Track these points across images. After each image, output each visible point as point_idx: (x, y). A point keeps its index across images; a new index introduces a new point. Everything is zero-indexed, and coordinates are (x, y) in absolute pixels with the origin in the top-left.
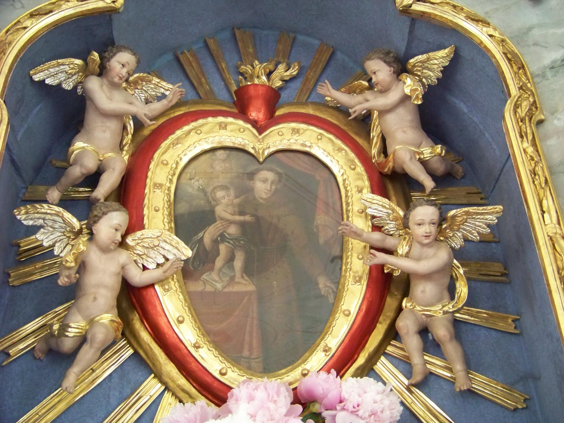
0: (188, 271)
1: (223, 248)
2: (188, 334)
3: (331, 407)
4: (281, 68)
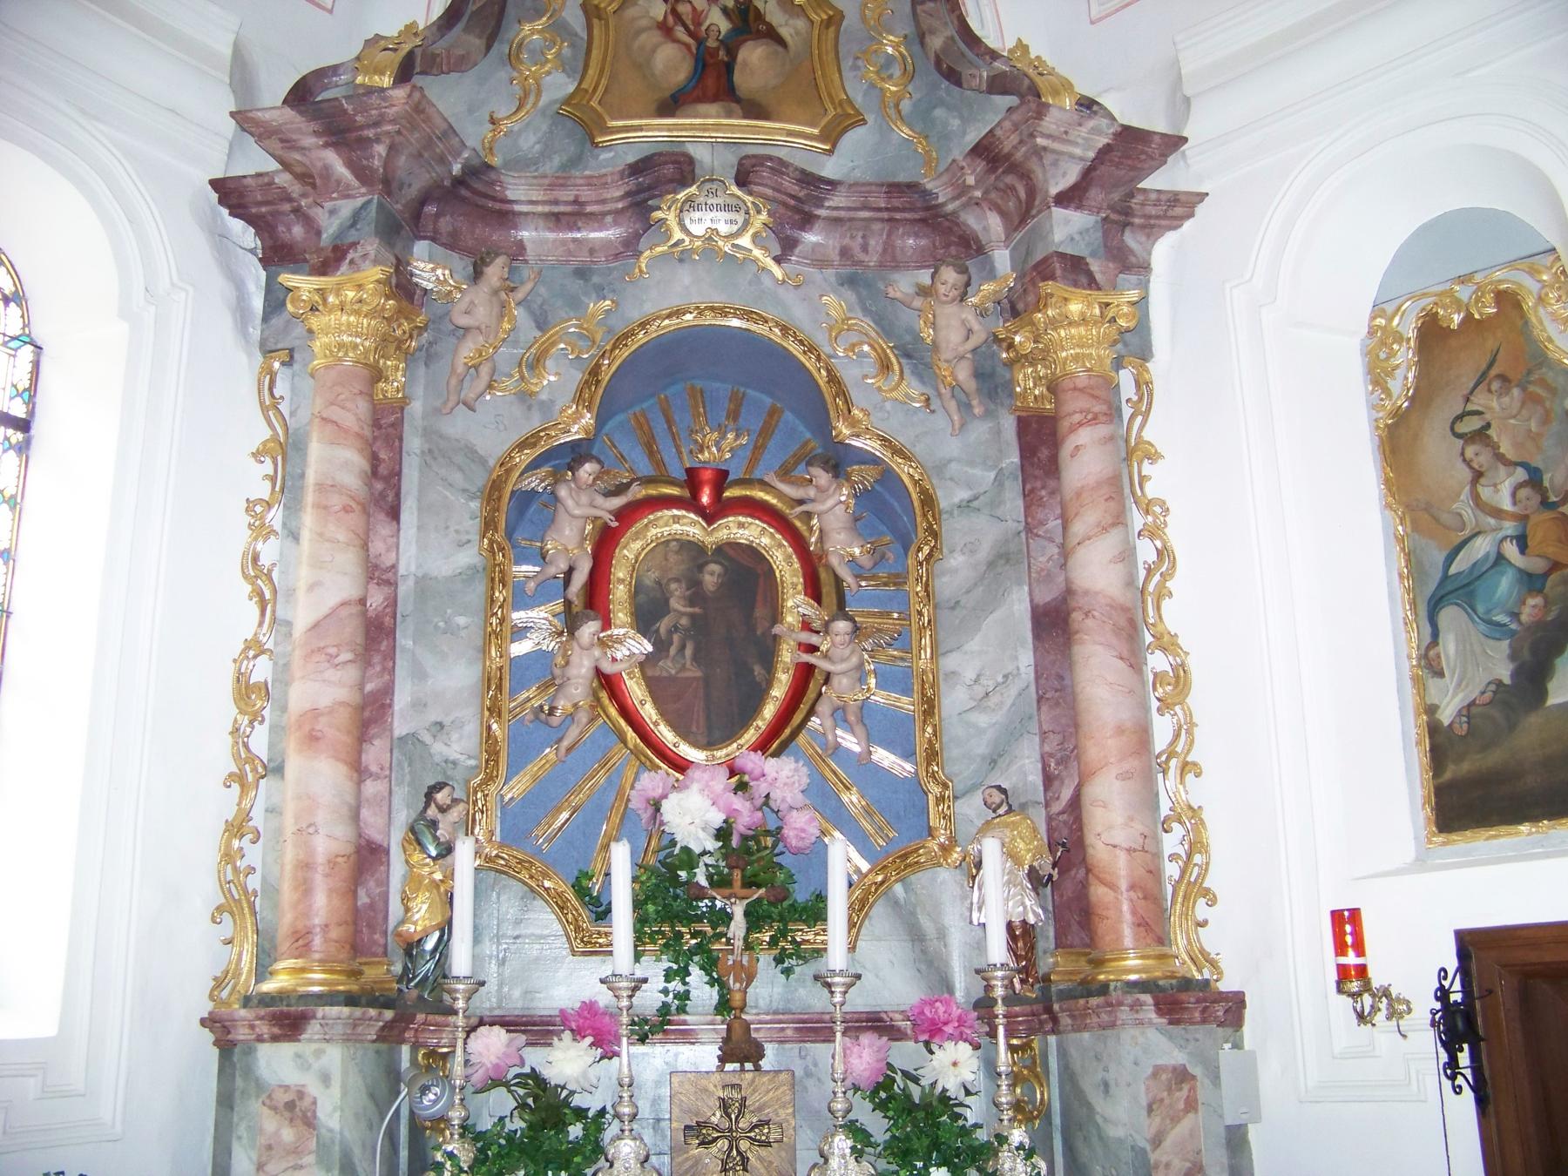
0: (646, 664)
1: (676, 637)
2: (649, 712)
3: (757, 779)
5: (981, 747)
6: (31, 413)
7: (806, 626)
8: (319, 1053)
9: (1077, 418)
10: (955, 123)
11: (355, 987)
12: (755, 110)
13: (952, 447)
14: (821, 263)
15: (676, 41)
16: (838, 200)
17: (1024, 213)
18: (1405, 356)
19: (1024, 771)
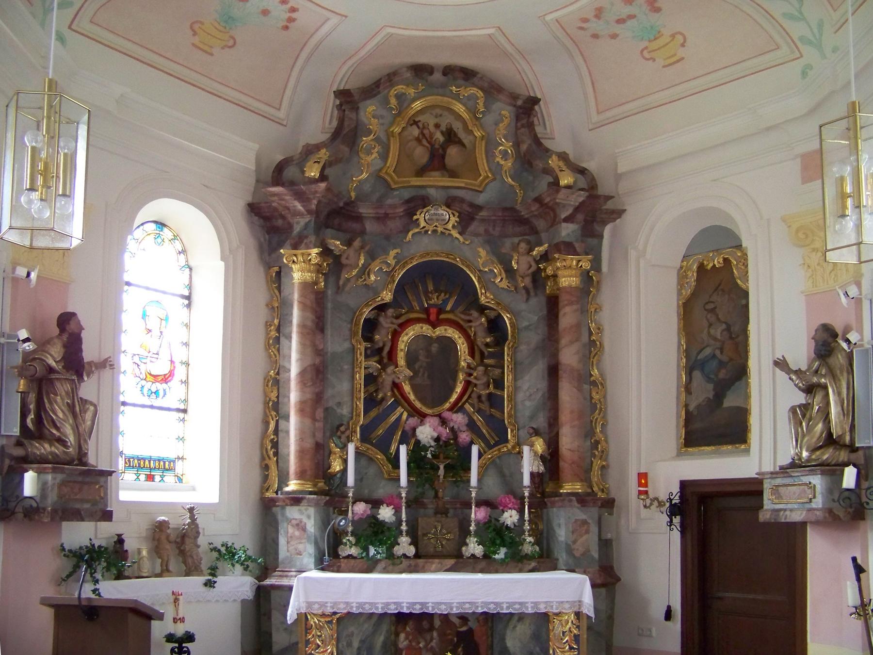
0: (411, 379)
1: (421, 370)
2: (412, 397)
4: (443, 294)
5: (528, 413)
6: (190, 293)
7: (469, 366)
8: (306, 510)
9: (566, 302)
10: (531, 178)
11: (316, 489)
12: (453, 174)
13: (523, 306)
14: (477, 235)
15: (423, 145)
16: (483, 214)
17: (554, 222)
18: (692, 276)
19: (541, 422)
